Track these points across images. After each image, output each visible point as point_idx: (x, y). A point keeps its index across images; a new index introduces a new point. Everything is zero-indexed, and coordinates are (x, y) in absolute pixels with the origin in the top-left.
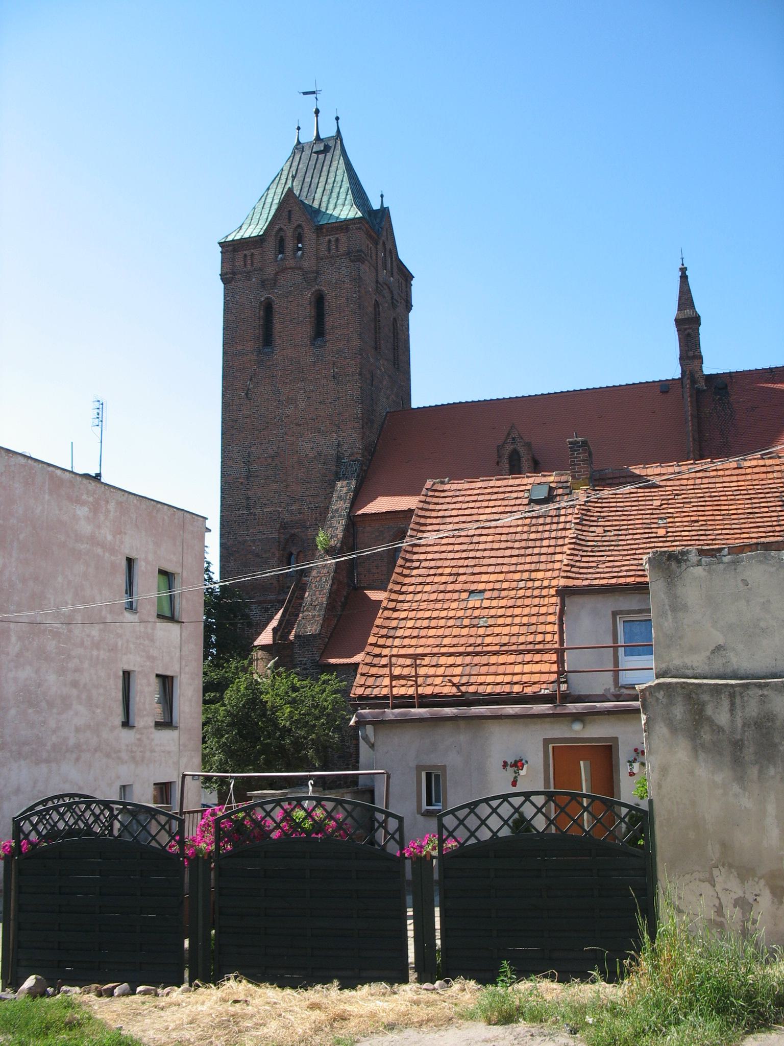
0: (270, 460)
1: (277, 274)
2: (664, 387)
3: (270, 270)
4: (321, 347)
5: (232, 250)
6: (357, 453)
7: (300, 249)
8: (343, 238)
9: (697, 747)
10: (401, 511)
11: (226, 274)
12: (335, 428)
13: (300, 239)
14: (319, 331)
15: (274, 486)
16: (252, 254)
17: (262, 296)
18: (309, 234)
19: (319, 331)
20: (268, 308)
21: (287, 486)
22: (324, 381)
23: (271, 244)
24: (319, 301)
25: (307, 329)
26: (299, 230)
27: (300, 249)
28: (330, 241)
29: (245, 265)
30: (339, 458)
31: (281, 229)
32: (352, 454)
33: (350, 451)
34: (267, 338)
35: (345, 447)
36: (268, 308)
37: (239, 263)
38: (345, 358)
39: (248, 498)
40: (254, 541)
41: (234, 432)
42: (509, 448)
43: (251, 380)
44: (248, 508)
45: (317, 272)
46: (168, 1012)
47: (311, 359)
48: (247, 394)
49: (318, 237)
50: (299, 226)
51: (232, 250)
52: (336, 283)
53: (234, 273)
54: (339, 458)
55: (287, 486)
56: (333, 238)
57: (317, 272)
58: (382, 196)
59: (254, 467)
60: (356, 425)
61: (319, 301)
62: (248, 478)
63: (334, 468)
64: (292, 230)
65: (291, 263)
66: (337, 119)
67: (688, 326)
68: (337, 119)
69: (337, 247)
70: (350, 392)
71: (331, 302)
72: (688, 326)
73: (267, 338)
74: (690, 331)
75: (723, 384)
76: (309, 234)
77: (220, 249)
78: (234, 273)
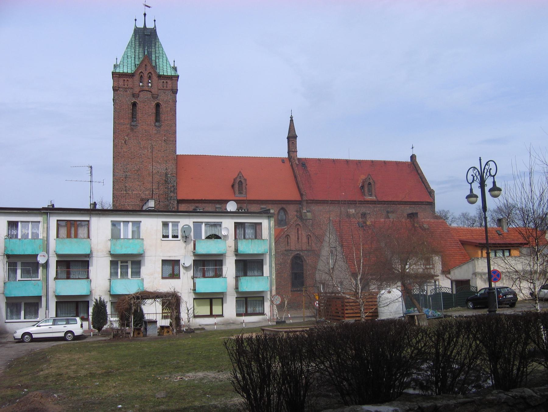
2: (283, 160)
3: (137, 90)
7: (149, 83)
8: (169, 82)
9: (481, 280)
13: (150, 78)
15: (138, 183)
18: (155, 78)
20: (134, 105)
21: (144, 183)
22: (160, 142)
23: (137, 77)
24: (158, 105)
25: (153, 118)
26: (150, 74)
27: (149, 83)
30: (166, 174)
31: (141, 72)
33: (171, 172)
34: (134, 116)
35: (169, 170)
36: (134, 105)
37: (121, 83)
40: (129, 205)
42: (238, 180)
46: (390, 306)
54: (166, 174)
55: (144, 183)
59: (128, 174)
61: (158, 105)
62: (126, 178)
63: (164, 178)
66: (155, 21)
67: (292, 138)
68: (155, 21)
72: (292, 138)
73: (134, 116)
75: (304, 163)
76: (155, 78)
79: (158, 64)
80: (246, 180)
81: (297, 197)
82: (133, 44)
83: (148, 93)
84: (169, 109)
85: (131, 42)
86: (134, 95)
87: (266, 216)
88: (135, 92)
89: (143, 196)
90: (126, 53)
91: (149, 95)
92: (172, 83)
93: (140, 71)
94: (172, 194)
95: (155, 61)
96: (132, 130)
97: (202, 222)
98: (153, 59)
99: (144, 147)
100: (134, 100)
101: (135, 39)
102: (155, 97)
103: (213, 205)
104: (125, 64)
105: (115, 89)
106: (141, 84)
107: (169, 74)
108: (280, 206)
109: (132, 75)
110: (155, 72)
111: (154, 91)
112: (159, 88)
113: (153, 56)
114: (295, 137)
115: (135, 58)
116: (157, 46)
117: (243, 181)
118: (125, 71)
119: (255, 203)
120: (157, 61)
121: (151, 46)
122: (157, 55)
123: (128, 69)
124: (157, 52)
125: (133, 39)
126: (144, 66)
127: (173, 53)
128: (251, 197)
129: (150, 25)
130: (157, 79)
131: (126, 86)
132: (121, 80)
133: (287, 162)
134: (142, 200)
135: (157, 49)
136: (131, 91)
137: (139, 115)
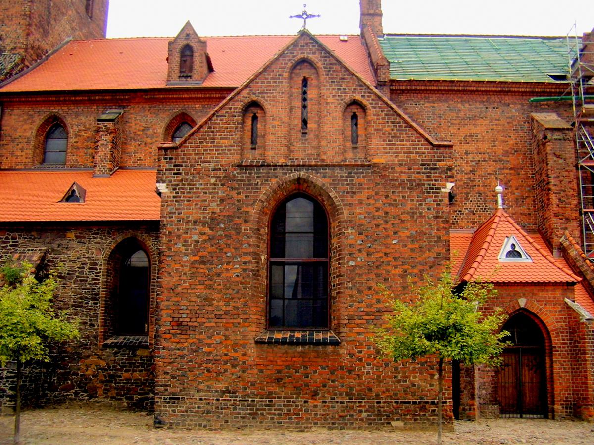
6: (20, 48)
33: (12, 45)
42: (182, 42)
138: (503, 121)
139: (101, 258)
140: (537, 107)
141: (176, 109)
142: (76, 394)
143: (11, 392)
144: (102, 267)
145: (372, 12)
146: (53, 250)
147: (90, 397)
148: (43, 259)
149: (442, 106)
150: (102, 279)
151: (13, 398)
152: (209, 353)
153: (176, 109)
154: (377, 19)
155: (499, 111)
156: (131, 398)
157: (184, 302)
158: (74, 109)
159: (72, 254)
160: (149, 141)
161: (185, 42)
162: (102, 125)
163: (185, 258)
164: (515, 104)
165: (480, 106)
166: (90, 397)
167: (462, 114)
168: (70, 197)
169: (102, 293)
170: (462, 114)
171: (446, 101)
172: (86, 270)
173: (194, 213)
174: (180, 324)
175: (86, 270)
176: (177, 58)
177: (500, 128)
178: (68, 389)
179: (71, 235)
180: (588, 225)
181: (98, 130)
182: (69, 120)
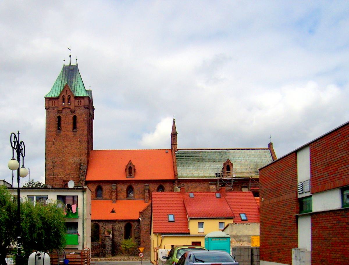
0: (60, 163)
1: (62, 109)
4: (75, 132)
5: (48, 99)
6: (86, 163)
8: (82, 100)
10: (296, 162)
11: (47, 107)
12: (79, 156)
13: (69, 99)
14: (75, 127)
15: (61, 170)
16: (55, 102)
17: (58, 115)
19: (75, 127)
20: (59, 118)
23: (61, 99)
24: (75, 118)
25: (71, 126)
26: (69, 97)
28: (78, 101)
29: (52, 105)
30: (80, 164)
31: (64, 96)
32: (84, 163)
33: (83, 162)
35: (82, 161)
36: (59, 118)
37: (51, 104)
38: (83, 136)
39: (54, 173)
41: (49, 154)
42: (129, 166)
43: (54, 139)
44: (53, 175)
45: (75, 110)
47: (72, 135)
48: (53, 143)
49: (75, 99)
50: (69, 96)
51: (48, 99)
52: (80, 114)
53: (49, 107)
56: (79, 100)
57: (257, 249)
58: (90, 86)
59: (56, 164)
60: (85, 155)
61: (75, 118)
64: (67, 96)
65: (67, 106)
66: (77, 60)
69: (81, 103)
70: (84, 146)
71: (79, 119)
74: (175, 137)
76: (72, 99)
77: (45, 99)
78: (49, 107)
79: (76, 89)
80: (134, 166)
81: (172, 177)
82: (61, 77)
83: (68, 109)
84: (82, 119)
85: (60, 76)
86: (59, 112)
87: (81, 191)
88: (59, 110)
89: (65, 179)
90: (56, 83)
91: (69, 111)
92: (84, 101)
93: (63, 95)
94: (82, 177)
95: (74, 87)
96: (57, 135)
97: (34, 196)
98: (73, 85)
99: (65, 146)
100: (59, 115)
101: (63, 73)
102: (73, 112)
103: (111, 184)
104: (54, 91)
105: (47, 108)
106: (63, 104)
107: (82, 95)
108: (159, 184)
109: (57, 98)
110: (73, 94)
111: (72, 107)
112: (76, 106)
113: (73, 84)
114: (176, 134)
115: (61, 86)
116: (77, 77)
117: (132, 167)
118: (53, 96)
119: (140, 182)
120: (76, 87)
121: (73, 77)
122: (76, 83)
123: (55, 94)
124: (77, 81)
125: (62, 74)
126: (65, 91)
127: (88, 82)
128: (137, 178)
129: (73, 63)
130: (74, 99)
131: (54, 106)
132: (51, 102)
133: (170, 153)
134: (64, 181)
135: (77, 79)
136: (57, 109)
137: (62, 124)
138: (203, 188)
139: (123, 227)
140: (211, 184)
141: (129, 184)
142: (120, 253)
143: (111, 253)
144: (123, 228)
145: (174, 144)
146: (114, 225)
147: (122, 254)
148: (112, 227)
149: (189, 184)
150: (123, 231)
151: (111, 254)
152: (148, 246)
153: (129, 184)
154: (176, 146)
155: (202, 185)
156: (130, 254)
157: (145, 238)
158: (104, 184)
159: (117, 226)
160: (123, 192)
161: (130, 166)
162: (113, 190)
163: (144, 231)
164: (206, 183)
165: (198, 184)
166: (122, 254)
167: (194, 186)
168: (113, 212)
169: (124, 234)
170: (194, 186)
171: (190, 183)
172: (120, 229)
173: (146, 223)
174: (144, 241)
175: (120, 229)
176: (128, 170)
177: (202, 189)
178: (118, 252)
179: (117, 222)
180: (254, 183)
181: (112, 191)
182: (103, 187)
